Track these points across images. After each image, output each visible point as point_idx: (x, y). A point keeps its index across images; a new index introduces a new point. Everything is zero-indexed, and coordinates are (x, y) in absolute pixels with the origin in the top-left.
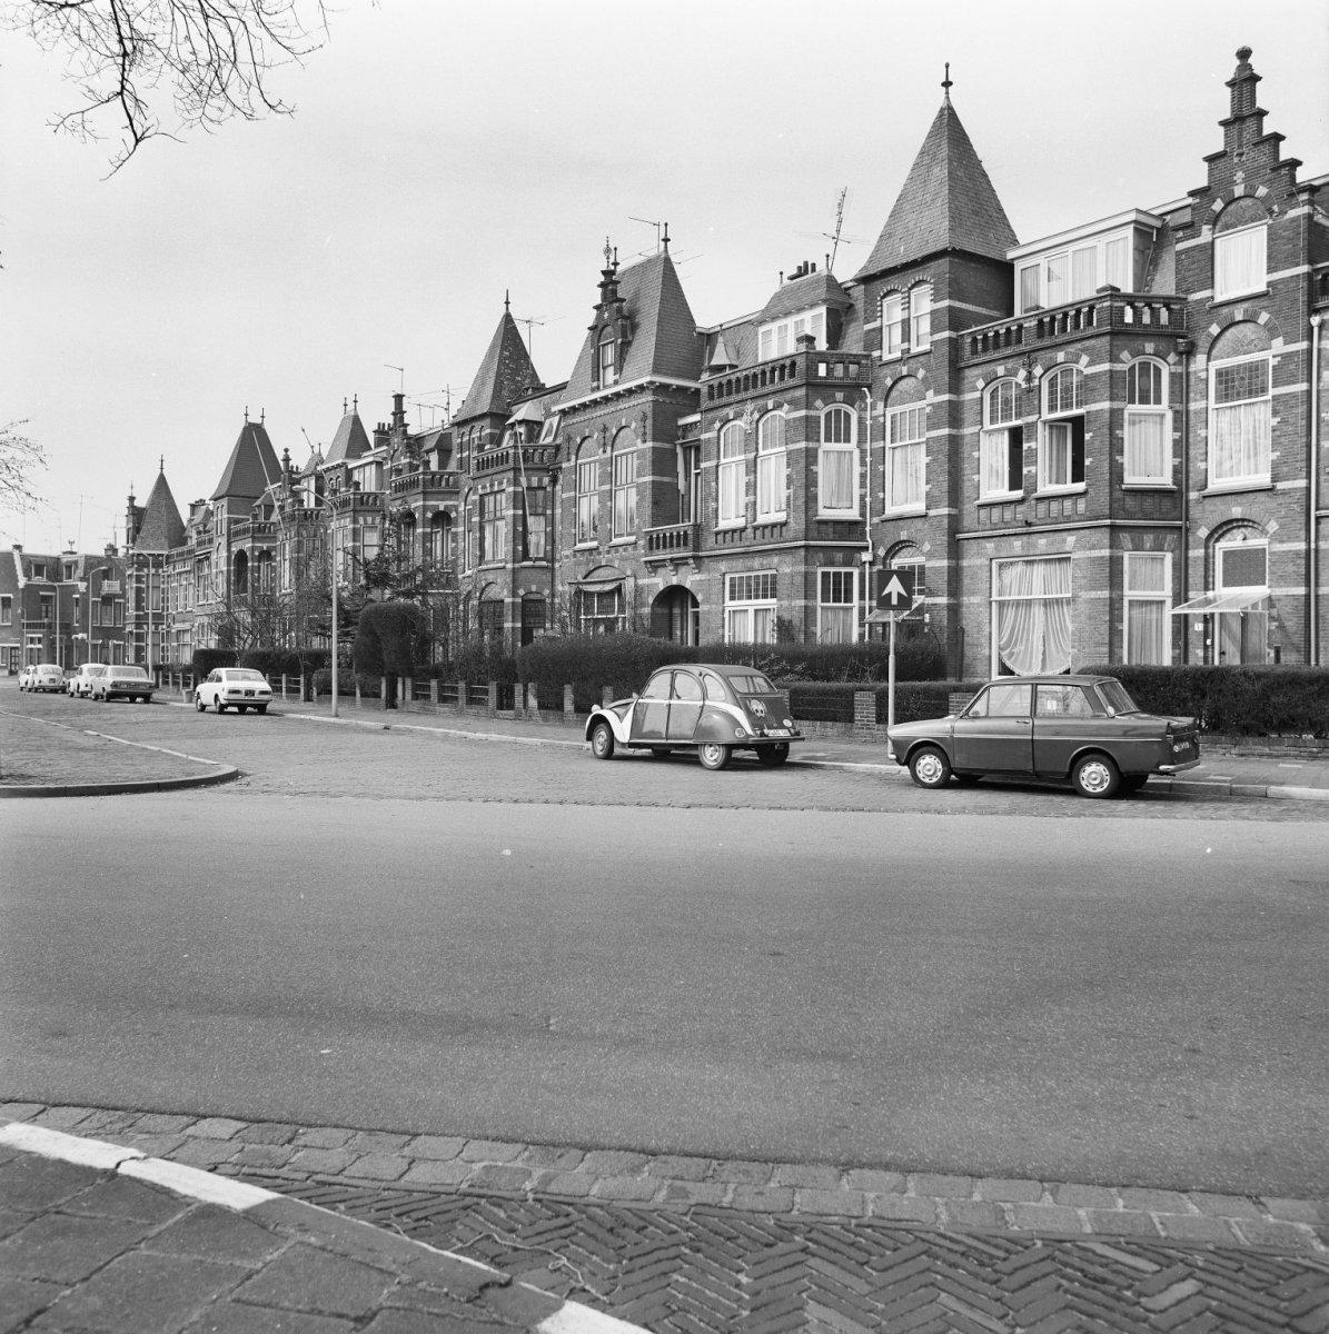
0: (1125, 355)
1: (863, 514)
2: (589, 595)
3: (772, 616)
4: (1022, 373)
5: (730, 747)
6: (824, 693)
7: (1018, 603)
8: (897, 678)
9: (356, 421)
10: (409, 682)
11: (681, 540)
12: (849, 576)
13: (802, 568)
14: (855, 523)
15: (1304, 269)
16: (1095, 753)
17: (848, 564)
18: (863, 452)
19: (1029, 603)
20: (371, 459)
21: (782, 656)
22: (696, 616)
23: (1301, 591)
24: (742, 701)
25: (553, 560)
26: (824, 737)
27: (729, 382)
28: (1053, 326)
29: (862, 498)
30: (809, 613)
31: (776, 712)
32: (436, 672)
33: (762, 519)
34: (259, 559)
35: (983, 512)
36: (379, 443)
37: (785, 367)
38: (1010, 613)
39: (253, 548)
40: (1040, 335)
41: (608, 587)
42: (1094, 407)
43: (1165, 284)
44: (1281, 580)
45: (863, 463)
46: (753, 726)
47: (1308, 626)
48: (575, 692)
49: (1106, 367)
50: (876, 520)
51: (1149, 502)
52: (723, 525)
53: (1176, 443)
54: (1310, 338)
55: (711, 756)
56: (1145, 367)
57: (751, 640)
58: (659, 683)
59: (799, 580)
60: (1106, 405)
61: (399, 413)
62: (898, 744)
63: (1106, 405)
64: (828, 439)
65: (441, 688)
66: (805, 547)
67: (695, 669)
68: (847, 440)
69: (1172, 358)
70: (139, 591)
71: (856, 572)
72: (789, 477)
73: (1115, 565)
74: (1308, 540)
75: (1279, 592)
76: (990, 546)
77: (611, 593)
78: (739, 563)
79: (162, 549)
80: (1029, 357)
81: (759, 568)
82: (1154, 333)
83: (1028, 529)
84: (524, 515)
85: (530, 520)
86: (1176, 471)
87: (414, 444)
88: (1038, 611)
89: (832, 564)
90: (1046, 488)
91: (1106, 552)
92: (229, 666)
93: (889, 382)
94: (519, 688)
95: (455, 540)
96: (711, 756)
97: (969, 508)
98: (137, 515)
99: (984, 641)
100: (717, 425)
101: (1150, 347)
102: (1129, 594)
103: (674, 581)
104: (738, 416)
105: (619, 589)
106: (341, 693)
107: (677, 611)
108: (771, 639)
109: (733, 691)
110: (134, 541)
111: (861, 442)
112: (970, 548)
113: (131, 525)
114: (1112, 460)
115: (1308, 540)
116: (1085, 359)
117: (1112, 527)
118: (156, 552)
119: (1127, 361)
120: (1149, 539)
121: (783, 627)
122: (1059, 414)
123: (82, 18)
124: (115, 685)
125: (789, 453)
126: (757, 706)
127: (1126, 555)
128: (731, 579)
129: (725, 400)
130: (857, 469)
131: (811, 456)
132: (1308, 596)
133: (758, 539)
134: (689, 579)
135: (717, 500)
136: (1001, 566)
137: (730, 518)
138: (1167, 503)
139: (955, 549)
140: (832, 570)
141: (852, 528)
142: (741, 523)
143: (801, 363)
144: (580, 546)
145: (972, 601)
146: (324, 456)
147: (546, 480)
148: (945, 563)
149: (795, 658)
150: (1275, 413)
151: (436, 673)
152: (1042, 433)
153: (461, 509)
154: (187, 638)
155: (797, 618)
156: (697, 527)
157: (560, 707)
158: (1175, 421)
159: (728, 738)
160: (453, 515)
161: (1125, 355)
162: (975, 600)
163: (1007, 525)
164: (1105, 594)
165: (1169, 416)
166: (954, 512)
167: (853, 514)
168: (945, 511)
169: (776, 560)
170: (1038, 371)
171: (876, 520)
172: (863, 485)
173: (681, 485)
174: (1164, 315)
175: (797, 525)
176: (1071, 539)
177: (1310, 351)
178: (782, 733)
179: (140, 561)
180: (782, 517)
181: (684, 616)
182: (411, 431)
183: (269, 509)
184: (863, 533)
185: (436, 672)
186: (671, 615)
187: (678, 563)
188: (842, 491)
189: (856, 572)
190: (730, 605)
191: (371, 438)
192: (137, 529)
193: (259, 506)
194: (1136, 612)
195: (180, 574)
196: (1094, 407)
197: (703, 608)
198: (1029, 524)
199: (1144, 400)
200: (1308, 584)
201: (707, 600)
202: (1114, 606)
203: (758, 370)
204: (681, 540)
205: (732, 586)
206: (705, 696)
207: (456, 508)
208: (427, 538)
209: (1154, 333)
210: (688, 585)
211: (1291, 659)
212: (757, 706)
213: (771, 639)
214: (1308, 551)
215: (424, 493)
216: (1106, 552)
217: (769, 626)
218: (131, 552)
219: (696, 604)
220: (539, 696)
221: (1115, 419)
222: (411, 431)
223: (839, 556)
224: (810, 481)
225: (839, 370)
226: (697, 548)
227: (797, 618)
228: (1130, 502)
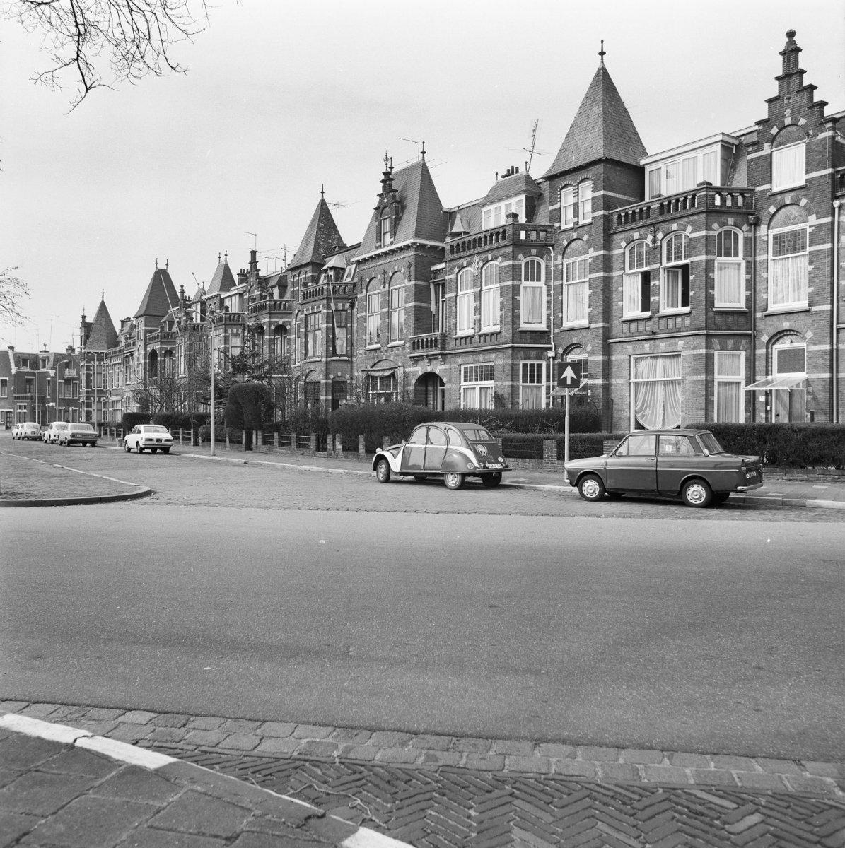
0: (715, 226)
1: (549, 327)
2: (374, 378)
3: (491, 392)
4: (650, 237)
5: (464, 475)
6: (524, 440)
7: (647, 384)
8: (571, 431)
9: (227, 268)
10: (260, 433)
11: (433, 343)
12: (540, 366)
13: (510, 361)
14: (544, 332)
15: (829, 171)
16: (696, 479)
17: (539, 358)
18: (549, 287)
19: (654, 383)
20: (236, 292)
21: (497, 417)
22: (443, 392)
23: (827, 375)
24: (472, 445)
25: (352, 356)
26: (524, 469)
27: (464, 243)
28: (670, 207)
29: (548, 316)
30: (514, 389)
31: (493, 452)
33: (484, 330)
34: (165, 355)
35: (625, 326)
36: (241, 282)
37: (499, 233)
38: (642, 390)
39: (161, 349)
40: (661, 213)
41: (387, 373)
42: (696, 259)
43: (741, 180)
44: (815, 368)
45: (549, 294)
46: (479, 461)
47: (831, 398)
48: (366, 440)
49: (703, 233)
50: (557, 331)
51: (730, 319)
52: (460, 334)
53: (748, 281)
54: (833, 215)
55: (452, 481)
56: (728, 233)
57: (477, 407)
58: (419, 434)
59: (508, 369)
60: (703, 257)
61: (254, 262)
62: (571, 473)
63: (703, 257)
64: (526, 279)
65: (281, 438)
66: (512, 348)
67: (442, 425)
68: (539, 280)
69: (745, 227)
70: (88, 376)
71: (544, 364)
72: (502, 303)
73: (709, 359)
74: (832, 343)
75: (813, 376)
76: (629, 347)
77: (388, 377)
78: (470, 358)
79: (103, 349)
80: (654, 227)
81: (483, 361)
82: (734, 211)
83: (654, 336)
84: (333, 328)
85: (337, 330)
86: (748, 299)
87: (263, 282)
88: (660, 389)
89: (529, 359)
90: (665, 310)
91: (703, 351)
92: (146, 424)
93: (565, 243)
94: (330, 437)
95: (289, 343)
96: (452, 481)
97: (616, 323)
98: (87, 327)
99: (626, 408)
100: (456, 270)
101: (731, 221)
102: (718, 377)
103: (429, 369)
104: (469, 264)
105: (393, 375)
106: (217, 440)
107: (430, 388)
108: (490, 406)
109: (466, 439)
110: (85, 344)
111: (547, 281)
112: (617, 349)
113: (83, 334)
114: (707, 292)
115: (832, 343)
116: (690, 228)
117: (707, 335)
118: (99, 351)
119: (716, 229)
120: (730, 343)
121: (498, 399)
122: (674, 263)
123: (52, 12)
124: (73, 435)
125: (502, 288)
126: (481, 449)
127: (716, 353)
128: (465, 368)
129: (461, 254)
130: (545, 298)
131: (515, 290)
132: (831, 379)
133: (482, 343)
134: (438, 368)
135: (456, 318)
136: (636, 360)
137: (464, 329)
138: (742, 320)
139: (607, 349)
140: (529, 362)
141: (542, 336)
142: (471, 332)
143: (509, 231)
144: (369, 347)
145: (618, 382)
146: (206, 290)
147: (347, 305)
148: (601, 358)
149: (505, 418)
150: (811, 263)
151: (277, 428)
152: (663, 275)
153: (293, 323)
154: (119, 405)
155: (507, 393)
156: (443, 335)
157: (356, 449)
158: (747, 268)
159: (463, 469)
160: (288, 327)
161: (715, 226)
162: (620, 381)
163: (640, 334)
164: (703, 377)
165: (744, 264)
166: (606, 325)
167: (542, 327)
168: (601, 325)
169: (493, 356)
170: (660, 236)
171: (557, 331)
172: (549, 308)
173: (433, 308)
174: (740, 200)
175: (507, 334)
176: (681, 343)
177: (833, 223)
178: (497, 466)
179: (89, 357)
180: (497, 328)
181: (435, 391)
182: (262, 274)
183: (171, 323)
184: (549, 339)
185: (277, 427)
186: (427, 391)
187: (431, 358)
188: (535, 312)
189: (544, 364)
190: (464, 384)
191: (236, 278)
192: (87, 336)
193: (165, 322)
194: (722, 389)
195: (114, 365)
196: (696, 259)
197: (447, 387)
198: (654, 333)
199: (728, 254)
200: (832, 372)
201: (449, 382)
202: (708, 385)
203: (482, 235)
204: (433, 343)
205: (465, 372)
206: (448, 443)
207: (290, 323)
208: (272, 342)
209: (734, 211)
210: (437, 372)
211: (821, 419)
212: (481, 449)
213: (490, 406)
214: (832, 350)
215: (270, 313)
216: (703, 351)
217: (489, 398)
218: (83, 351)
219: (442, 384)
220: (343, 443)
221: (709, 267)
222: (262, 274)
223: (534, 353)
224: (515, 306)
225: (534, 235)
226: (443, 348)
227: (507, 393)
228: (718, 319)
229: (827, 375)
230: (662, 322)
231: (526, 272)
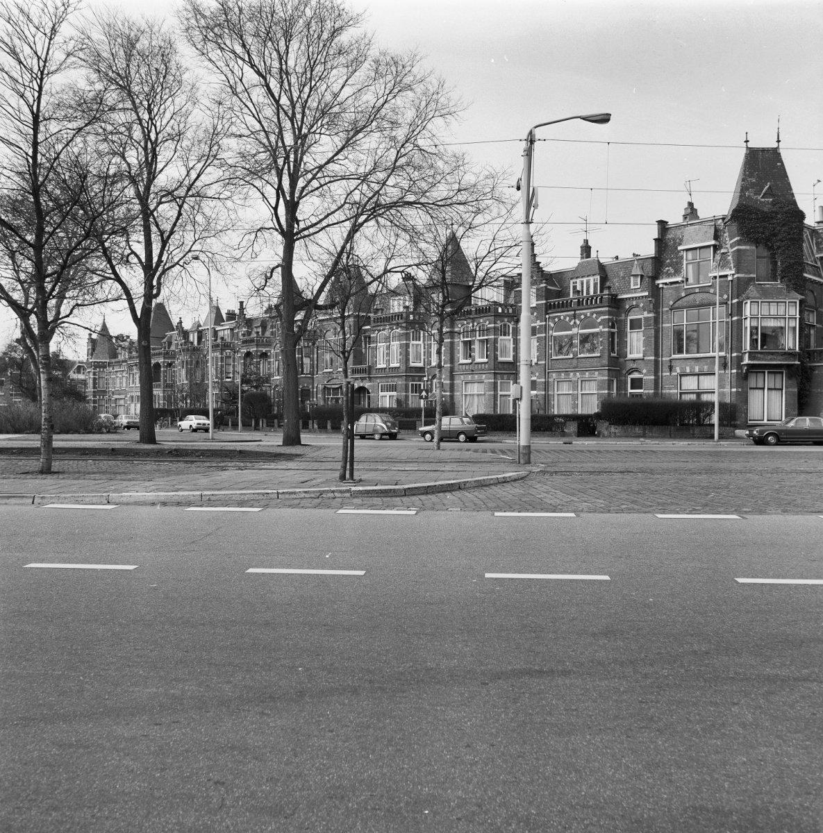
0: (499, 322)
1: (424, 365)
2: (329, 389)
3: (395, 398)
4: (471, 325)
5: (382, 434)
6: (408, 422)
7: (470, 395)
8: (425, 417)
9: (218, 309)
10: (265, 421)
11: (364, 371)
12: (420, 385)
13: (404, 382)
14: (422, 368)
15: (544, 302)
16: (462, 433)
17: (420, 381)
18: (424, 344)
19: (473, 395)
20: (228, 327)
21: (398, 411)
22: (369, 397)
23: (544, 393)
24: (385, 423)
25: (313, 375)
26: (408, 434)
27: (381, 318)
28: (482, 311)
29: (424, 359)
30: (407, 397)
31: (394, 426)
32: (31, 424)
33: (392, 365)
34: (167, 367)
35: (460, 366)
36: (229, 319)
37: (399, 315)
38: (468, 398)
39: (164, 362)
40: (476, 314)
41: (337, 386)
42: (490, 337)
43: (511, 301)
44: (540, 390)
45: (425, 348)
46: (388, 429)
47: (545, 403)
48: (332, 423)
49: (493, 325)
50: (429, 367)
51: (506, 366)
52: (379, 366)
53: (514, 348)
54: (546, 321)
55: (377, 437)
56: (505, 325)
57: (388, 406)
58: (363, 418)
59: (404, 386)
60: (493, 337)
61: (242, 308)
62: (421, 432)
63: (493, 337)
64: (413, 340)
65: (279, 422)
66: (406, 376)
67: (372, 414)
68: (420, 340)
69: (512, 323)
70: (94, 379)
71: (422, 384)
72: (400, 352)
73: (495, 384)
74: (545, 378)
75: (539, 393)
76: (462, 377)
77: (338, 388)
78: (384, 380)
79: (106, 359)
80: (473, 320)
81: (391, 382)
82: (508, 316)
83: (472, 372)
84: (302, 357)
85: (304, 359)
86: (514, 356)
87: (249, 322)
88: (476, 398)
89: (414, 381)
90: (478, 360)
91: (493, 381)
92: (812, 415)
93: (433, 322)
94: (310, 422)
95: (269, 363)
96: (377, 437)
97: (456, 364)
98: (93, 342)
99: (460, 407)
100: (377, 332)
101: (506, 320)
102: (500, 393)
103: (361, 385)
104: (384, 330)
105: (341, 387)
106: (244, 425)
107: (362, 395)
108: (395, 406)
109: (383, 420)
110: (92, 355)
111: (424, 341)
112: (456, 377)
113: (90, 347)
114: (495, 353)
115: (545, 378)
116: (488, 322)
117: (494, 373)
118: (103, 361)
119: (499, 324)
120: (505, 376)
121: (398, 401)
122: (481, 338)
123: (474, 493)
124: (128, 423)
125: (401, 344)
126: (389, 424)
127: (499, 382)
128: (382, 385)
129: (379, 324)
130: (422, 350)
131: (407, 346)
132: (545, 394)
133: (389, 372)
134: (367, 385)
135: (376, 357)
136: (466, 383)
137: (381, 365)
138: (511, 366)
139: (452, 378)
140: (414, 383)
141: (421, 369)
142: (384, 366)
143: (404, 315)
144: (325, 370)
145: (457, 394)
146: (202, 324)
147: (310, 344)
148: (449, 382)
149: (400, 412)
150: (538, 342)
151: (276, 417)
152: (477, 343)
153: (272, 351)
154: (122, 402)
155: (403, 399)
156: (370, 367)
157: (326, 427)
158: (513, 341)
159: (381, 432)
160: (269, 354)
161: (499, 322)
162: (458, 394)
163: (467, 370)
164: (492, 393)
165: (512, 340)
166: (452, 366)
167: (421, 365)
168: (449, 365)
169: (396, 379)
170: (475, 324)
171: (429, 367)
172: (424, 355)
173: (363, 350)
174: (511, 311)
175: (403, 368)
176: (484, 376)
177: (546, 325)
178: (395, 431)
179: (97, 365)
180: (398, 365)
181: (364, 397)
182: (247, 317)
183: (170, 344)
184: (425, 372)
185: (31, 424)
186: (360, 397)
187: (363, 379)
188: (418, 358)
189: (422, 384)
190: (381, 394)
191: (224, 316)
192: (93, 350)
193: (165, 343)
194: (502, 398)
195: (117, 372)
196: (490, 337)
197: (371, 395)
198: (472, 371)
199: (505, 335)
200: (545, 391)
201: (373, 392)
202: (495, 397)
203: (390, 315)
204: (364, 371)
205: (382, 387)
206: (375, 422)
207: (270, 351)
208: (258, 363)
209: (508, 316)
210: (366, 386)
211: (541, 412)
212: (389, 424)
213: (395, 406)
214: (545, 382)
215: (257, 345)
216: (493, 381)
217: (394, 401)
218: (90, 361)
219: (368, 393)
220: (318, 424)
222: (247, 317)
223: (417, 378)
224: (407, 354)
225: (417, 317)
226: (369, 374)
227: (403, 399)
228: (500, 366)
229: (544, 393)
230: (477, 365)
231: (413, 336)
